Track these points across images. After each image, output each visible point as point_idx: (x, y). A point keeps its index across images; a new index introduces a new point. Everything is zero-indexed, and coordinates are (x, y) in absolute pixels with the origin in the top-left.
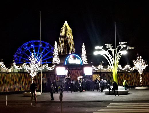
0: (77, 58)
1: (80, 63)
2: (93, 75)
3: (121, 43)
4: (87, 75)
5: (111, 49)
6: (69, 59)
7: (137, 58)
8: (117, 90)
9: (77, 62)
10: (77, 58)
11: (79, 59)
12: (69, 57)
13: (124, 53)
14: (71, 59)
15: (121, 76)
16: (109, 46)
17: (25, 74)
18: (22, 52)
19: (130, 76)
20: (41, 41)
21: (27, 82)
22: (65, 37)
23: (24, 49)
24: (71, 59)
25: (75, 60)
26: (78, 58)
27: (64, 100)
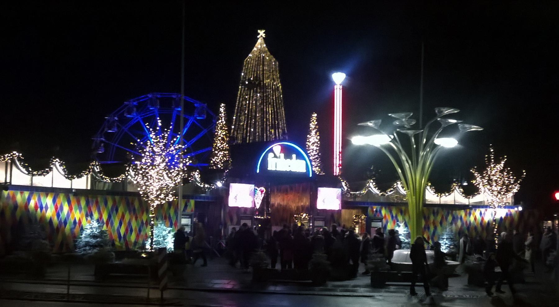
0: (294, 156)
1: (304, 171)
2: (343, 211)
3: (441, 112)
4: (324, 211)
5: (409, 129)
6: (271, 155)
7: (224, 122)
8: (426, 263)
9: (297, 166)
10: (294, 156)
11: (304, 159)
12: (271, 150)
13: (448, 143)
14: (275, 156)
15: (432, 218)
16: (246, 89)
17: (130, 198)
18: (118, 127)
19: (461, 218)
20: (183, 97)
21: (134, 224)
22: (256, 84)
23: (125, 117)
24: (275, 156)
25: (288, 160)
26: (299, 156)
27: (147, 290)
